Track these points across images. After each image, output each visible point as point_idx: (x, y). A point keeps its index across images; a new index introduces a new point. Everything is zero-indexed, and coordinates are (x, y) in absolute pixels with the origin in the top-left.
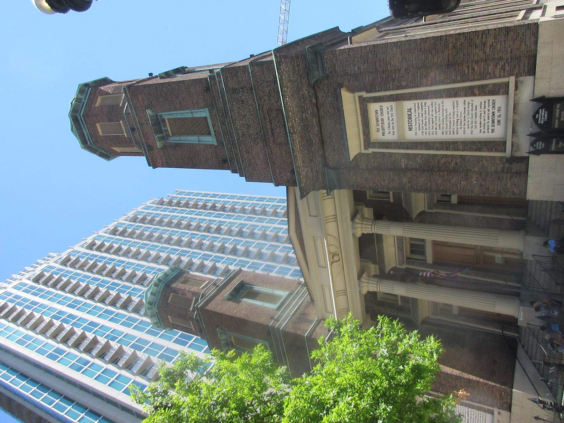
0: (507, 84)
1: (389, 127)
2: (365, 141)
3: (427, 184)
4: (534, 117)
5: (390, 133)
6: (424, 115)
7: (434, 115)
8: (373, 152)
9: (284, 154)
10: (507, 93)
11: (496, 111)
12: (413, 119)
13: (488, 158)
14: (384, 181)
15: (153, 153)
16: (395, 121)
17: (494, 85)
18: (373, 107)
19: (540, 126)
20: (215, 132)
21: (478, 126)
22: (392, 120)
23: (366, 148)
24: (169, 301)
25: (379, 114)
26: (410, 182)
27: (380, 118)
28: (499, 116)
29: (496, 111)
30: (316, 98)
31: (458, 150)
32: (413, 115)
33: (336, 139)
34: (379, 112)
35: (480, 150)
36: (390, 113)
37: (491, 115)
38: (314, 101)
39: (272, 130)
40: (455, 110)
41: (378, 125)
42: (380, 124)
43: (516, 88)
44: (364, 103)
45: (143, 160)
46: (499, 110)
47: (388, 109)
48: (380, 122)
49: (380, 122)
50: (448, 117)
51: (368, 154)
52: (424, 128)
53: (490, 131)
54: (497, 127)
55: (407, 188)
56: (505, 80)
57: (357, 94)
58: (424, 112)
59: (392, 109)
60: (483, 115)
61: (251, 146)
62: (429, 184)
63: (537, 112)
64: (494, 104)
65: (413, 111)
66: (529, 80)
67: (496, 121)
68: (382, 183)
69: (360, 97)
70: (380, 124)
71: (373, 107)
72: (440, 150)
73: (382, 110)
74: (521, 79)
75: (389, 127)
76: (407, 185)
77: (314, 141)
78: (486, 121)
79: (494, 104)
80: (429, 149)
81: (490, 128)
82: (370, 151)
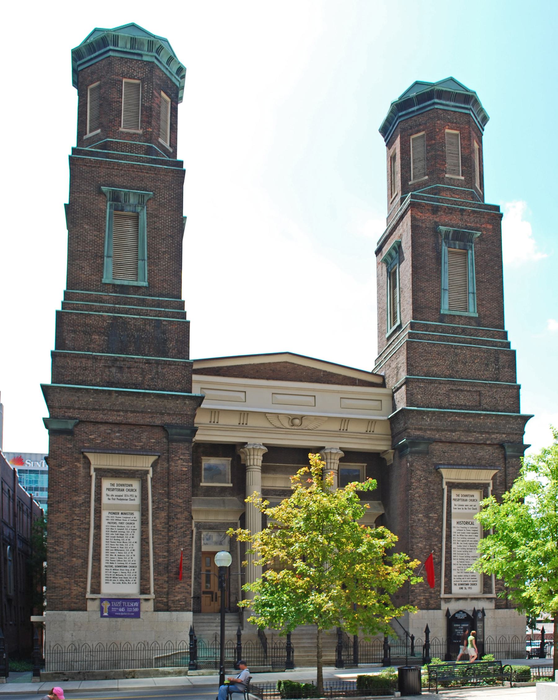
0: (491, 592)
1: (460, 505)
2: (453, 483)
3: (418, 535)
4: (461, 611)
5: (455, 505)
6: (468, 534)
7: (468, 542)
8: (443, 489)
9: (440, 397)
10: (485, 592)
11: (469, 586)
12: (466, 526)
13: (439, 582)
14: (419, 497)
15: (428, 210)
16: (465, 511)
17: (491, 585)
18: (136, 484)
19: (454, 615)
20: (454, 316)
21: (459, 574)
22: (466, 509)
23: (447, 483)
24: (163, 94)
25: (129, 488)
26: (419, 520)
27: (468, 498)
28: (465, 588)
29: (469, 586)
30: (489, 444)
31: (446, 561)
32: (469, 526)
33: (454, 456)
34: (472, 498)
35: (446, 576)
36: (471, 507)
37: (466, 583)
38: (488, 442)
39: (462, 391)
40: (471, 558)
41: (462, 496)
42: (118, 487)
43: (488, 599)
44: (141, 475)
45: (67, 202)
46: (469, 588)
47: (475, 506)
48: (121, 488)
49: (121, 488)
50: (466, 553)
51: (442, 484)
52: (459, 534)
53: (455, 583)
54: (458, 587)
55: (413, 517)
56: (494, 591)
57: (491, 482)
58: (470, 534)
59: (474, 509)
60: (467, 577)
61: (445, 360)
62: (418, 537)
63: (464, 612)
64: (474, 584)
65: (472, 526)
66: (492, 605)
67: (462, 586)
68: (417, 495)
69: (488, 484)
70: (118, 487)
71: (136, 484)
72: (446, 546)
73: (132, 490)
74: (494, 601)
75: (460, 505)
76: (416, 518)
77: (454, 434)
78: (462, 580)
79: (474, 584)
80: (446, 538)
81: (457, 583)
82: (445, 487)
